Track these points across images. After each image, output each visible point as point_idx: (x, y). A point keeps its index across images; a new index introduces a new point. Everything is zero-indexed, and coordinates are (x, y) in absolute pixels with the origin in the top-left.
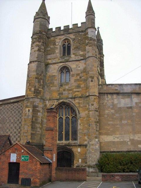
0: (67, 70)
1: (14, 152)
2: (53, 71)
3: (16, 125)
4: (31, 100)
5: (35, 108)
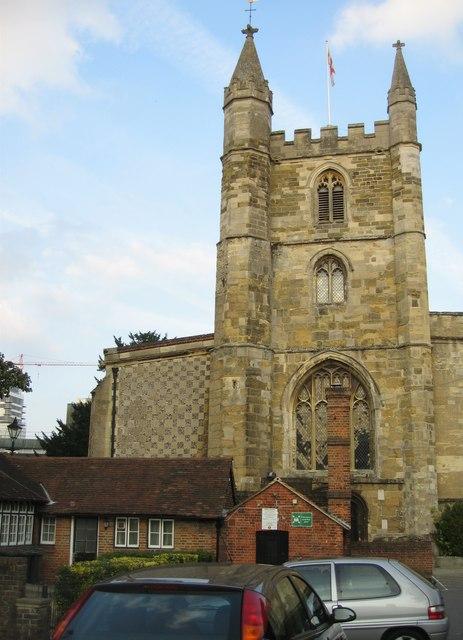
0: (334, 266)
1: (270, 505)
2: (295, 267)
3: (181, 423)
4: (241, 352)
5: (253, 377)
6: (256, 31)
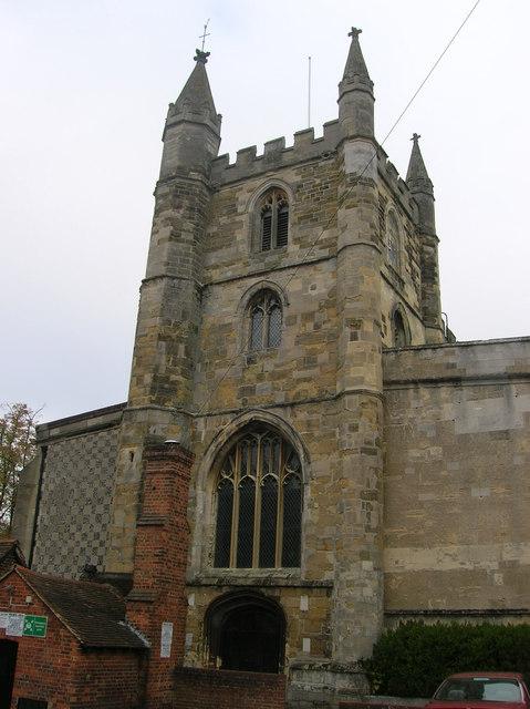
4: (141, 417)
6: (360, 31)
